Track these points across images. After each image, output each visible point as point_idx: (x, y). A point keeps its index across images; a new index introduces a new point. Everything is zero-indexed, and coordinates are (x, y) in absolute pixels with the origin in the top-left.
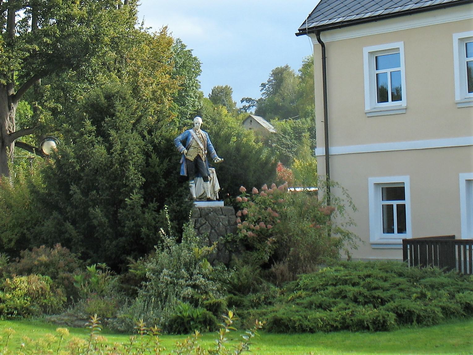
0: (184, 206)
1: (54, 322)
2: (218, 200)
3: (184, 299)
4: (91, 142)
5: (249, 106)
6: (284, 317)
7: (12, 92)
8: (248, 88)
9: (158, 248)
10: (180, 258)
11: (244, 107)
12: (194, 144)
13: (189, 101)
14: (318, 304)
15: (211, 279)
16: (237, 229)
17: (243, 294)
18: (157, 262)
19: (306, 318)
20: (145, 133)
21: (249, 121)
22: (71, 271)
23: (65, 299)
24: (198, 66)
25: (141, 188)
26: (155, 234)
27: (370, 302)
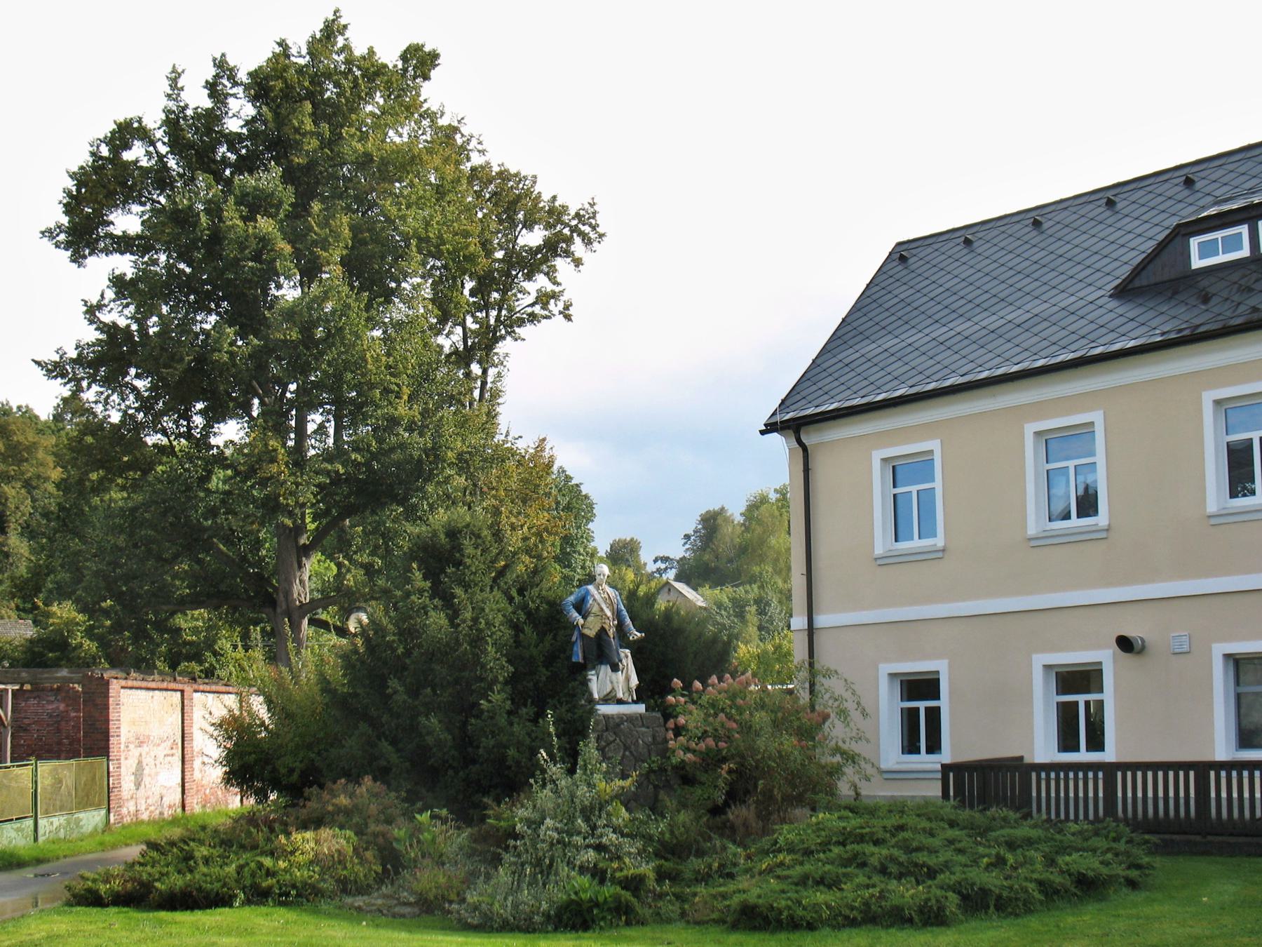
0: (579, 712)
1: (359, 909)
2: (634, 702)
3: (582, 870)
4: (423, 608)
5: (666, 569)
6: (760, 901)
7: (303, 540)
8: (665, 542)
9: (536, 782)
10: (577, 804)
11: (659, 570)
12: (595, 609)
13: (577, 560)
14: (817, 877)
15: (627, 835)
16: (667, 749)
17: (679, 857)
18: (535, 806)
19: (799, 903)
20: (514, 593)
21: (666, 589)
22: (389, 821)
23: (379, 869)
24: (591, 506)
25: (506, 683)
26: (530, 760)
27: (910, 873)
